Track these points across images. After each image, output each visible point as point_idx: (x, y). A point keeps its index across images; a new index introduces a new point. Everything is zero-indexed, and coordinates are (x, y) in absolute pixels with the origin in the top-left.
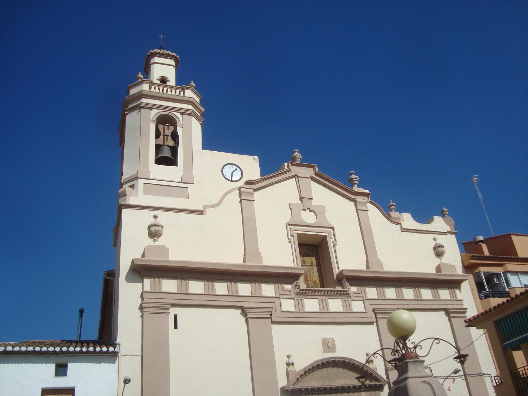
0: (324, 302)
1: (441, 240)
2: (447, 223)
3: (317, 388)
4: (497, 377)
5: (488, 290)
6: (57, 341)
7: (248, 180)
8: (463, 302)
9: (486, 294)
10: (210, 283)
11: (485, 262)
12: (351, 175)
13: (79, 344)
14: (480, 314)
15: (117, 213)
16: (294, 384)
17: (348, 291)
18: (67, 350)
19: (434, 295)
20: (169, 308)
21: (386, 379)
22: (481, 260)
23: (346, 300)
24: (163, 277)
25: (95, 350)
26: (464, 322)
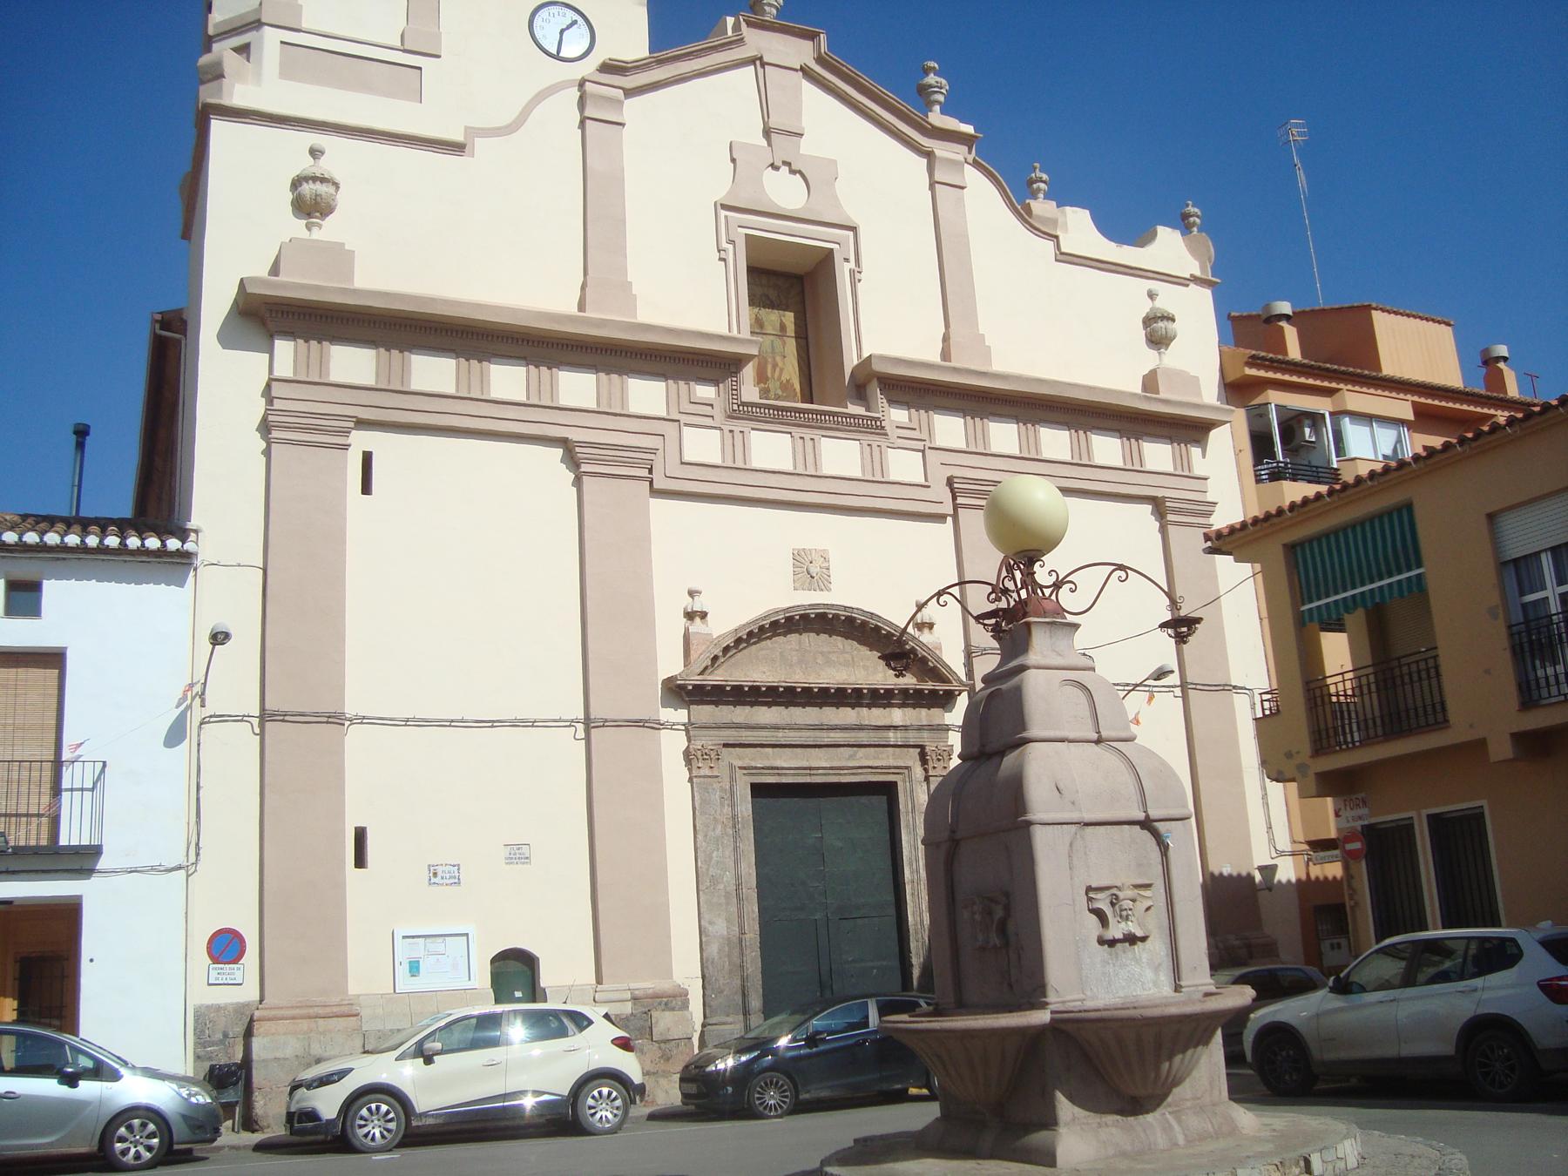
0: (809, 444)
1: (1170, 298)
2: (1193, 251)
3: (769, 688)
4: (1269, 696)
5: (1281, 459)
6: (8, 518)
7: (610, 59)
8: (1206, 484)
9: (1275, 467)
10: (474, 363)
11: (1287, 377)
12: (927, 75)
13: (77, 528)
14: (1250, 521)
15: (194, 131)
16: (702, 673)
17: (882, 418)
18: (38, 540)
19: (1128, 455)
20: (349, 432)
21: (964, 678)
22: (1276, 370)
23: (874, 445)
24: (334, 337)
25: (123, 544)
26: (1203, 538)
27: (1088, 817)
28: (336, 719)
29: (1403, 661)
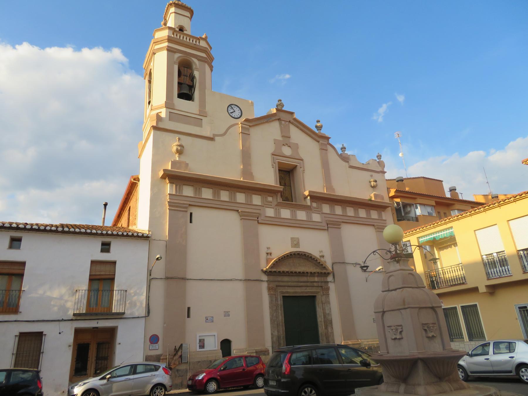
27: (421, 306)
28: (184, 279)
29: (452, 267)
